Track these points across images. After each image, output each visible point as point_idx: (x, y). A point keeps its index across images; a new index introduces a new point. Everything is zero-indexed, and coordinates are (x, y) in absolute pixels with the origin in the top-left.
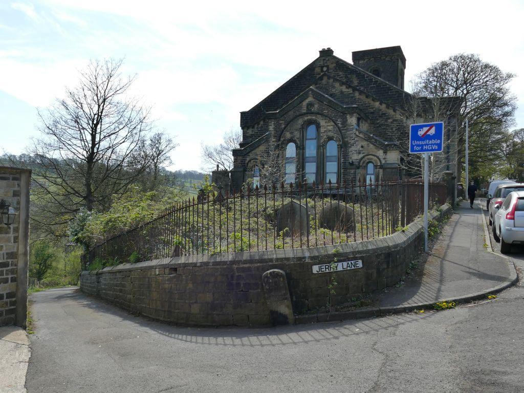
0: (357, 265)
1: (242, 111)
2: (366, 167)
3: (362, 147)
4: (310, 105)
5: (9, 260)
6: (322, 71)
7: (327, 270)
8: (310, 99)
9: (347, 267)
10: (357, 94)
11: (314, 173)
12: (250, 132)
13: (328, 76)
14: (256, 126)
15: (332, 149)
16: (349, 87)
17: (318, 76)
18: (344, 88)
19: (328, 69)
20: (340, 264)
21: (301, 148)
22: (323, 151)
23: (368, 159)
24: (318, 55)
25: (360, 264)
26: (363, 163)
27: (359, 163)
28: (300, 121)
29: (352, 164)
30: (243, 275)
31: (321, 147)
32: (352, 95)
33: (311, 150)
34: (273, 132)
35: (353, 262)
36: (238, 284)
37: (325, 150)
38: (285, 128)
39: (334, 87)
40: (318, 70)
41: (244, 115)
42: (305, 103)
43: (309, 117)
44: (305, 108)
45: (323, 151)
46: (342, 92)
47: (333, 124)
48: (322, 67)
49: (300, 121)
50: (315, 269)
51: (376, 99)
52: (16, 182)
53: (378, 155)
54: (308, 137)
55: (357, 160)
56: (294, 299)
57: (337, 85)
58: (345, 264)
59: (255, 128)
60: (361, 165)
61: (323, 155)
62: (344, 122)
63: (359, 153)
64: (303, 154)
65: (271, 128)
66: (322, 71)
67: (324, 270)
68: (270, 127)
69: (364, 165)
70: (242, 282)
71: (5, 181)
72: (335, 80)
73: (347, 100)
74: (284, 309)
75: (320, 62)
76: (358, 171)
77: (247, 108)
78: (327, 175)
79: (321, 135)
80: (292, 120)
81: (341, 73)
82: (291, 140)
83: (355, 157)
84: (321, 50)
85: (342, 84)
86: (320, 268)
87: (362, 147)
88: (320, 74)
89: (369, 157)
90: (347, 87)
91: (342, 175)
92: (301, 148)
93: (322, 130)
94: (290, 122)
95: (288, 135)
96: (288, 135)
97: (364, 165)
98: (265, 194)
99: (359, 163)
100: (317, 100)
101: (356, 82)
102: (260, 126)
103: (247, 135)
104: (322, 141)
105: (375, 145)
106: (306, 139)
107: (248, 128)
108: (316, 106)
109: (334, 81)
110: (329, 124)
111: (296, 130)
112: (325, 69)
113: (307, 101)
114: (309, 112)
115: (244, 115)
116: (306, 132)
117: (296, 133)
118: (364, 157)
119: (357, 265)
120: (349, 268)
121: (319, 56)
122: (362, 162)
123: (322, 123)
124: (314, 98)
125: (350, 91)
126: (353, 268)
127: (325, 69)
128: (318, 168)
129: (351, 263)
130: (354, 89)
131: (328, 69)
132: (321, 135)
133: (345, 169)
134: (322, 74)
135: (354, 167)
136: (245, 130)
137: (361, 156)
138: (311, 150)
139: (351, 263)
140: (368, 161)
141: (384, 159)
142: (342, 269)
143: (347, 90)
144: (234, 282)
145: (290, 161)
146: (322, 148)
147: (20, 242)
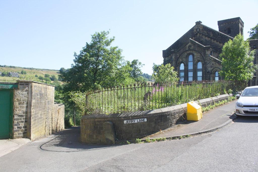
0: (144, 121)
1: (163, 50)
2: (215, 74)
3: (213, 64)
4: (190, 46)
5: (24, 114)
6: (197, 31)
7: (132, 122)
8: (190, 44)
9: (140, 121)
10: (212, 40)
11: (192, 77)
12: (167, 59)
13: (199, 33)
14: (169, 56)
15: (200, 66)
16: (209, 37)
17: (195, 33)
18: (207, 38)
19: (199, 30)
20: (136, 120)
21: (186, 66)
22: (196, 67)
23: (216, 70)
24: (195, 24)
25: (146, 120)
26: (213, 72)
27: (211, 71)
28: (186, 54)
29: (208, 72)
30: (98, 123)
31: (195, 65)
32: (210, 41)
33: (191, 67)
34: (174, 59)
35: (142, 119)
36: (97, 127)
37: (197, 66)
38: (179, 57)
39: (202, 38)
40: (195, 30)
41: (164, 52)
42: (187, 46)
43: (190, 52)
44: (188, 48)
45: (196, 67)
46: (206, 40)
47: (200, 54)
48: (197, 29)
49: (186, 54)
50: (125, 122)
51: (221, 42)
52: (27, 86)
53: (220, 68)
54: (189, 61)
55: (211, 70)
56: (117, 134)
57: (204, 37)
58: (138, 120)
59: (169, 57)
60: (212, 72)
61: (196, 69)
62: (205, 54)
63: (212, 67)
64: (187, 68)
65: (173, 57)
66: (197, 31)
67: (129, 122)
68: (173, 57)
69: (214, 72)
70: (98, 126)
71: (22, 86)
72: (203, 35)
73: (208, 43)
74: (111, 138)
75: (196, 27)
76: (211, 75)
77: (165, 48)
78: (198, 77)
79: (195, 60)
80: (182, 54)
81: (205, 32)
82: (182, 62)
83: (210, 69)
84: (196, 22)
85: (206, 36)
86: (127, 122)
87: (213, 64)
88: (196, 32)
89: (216, 69)
90: (208, 38)
91: (204, 77)
92: (186, 66)
93: (195, 57)
94: (181, 54)
95: (181, 60)
96: (181, 60)
97: (214, 72)
98: (134, 88)
99: (211, 71)
100: (193, 44)
101: (212, 35)
102: (171, 56)
103: (166, 60)
104: (195, 62)
105: (218, 63)
106: (189, 62)
107: (166, 57)
108: (192, 47)
109: (202, 35)
110: (198, 55)
111: (184, 58)
112: (198, 30)
113: (189, 44)
114: (189, 50)
115: (164, 52)
116: (189, 58)
117: (184, 59)
118: (213, 69)
119: (144, 121)
120: (140, 122)
121: (195, 25)
122: (213, 71)
123: (195, 54)
124: (191, 43)
125: (209, 39)
126: (142, 122)
127: (198, 30)
128: (185, 74)
129: (141, 120)
130: (211, 38)
131: (199, 30)
132: (195, 60)
133: (205, 74)
134: (197, 32)
135: (209, 73)
136: (165, 58)
137: (212, 68)
138: (191, 67)
139: (141, 120)
140: (215, 71)
142: (137, 122)
143: (208, 39)
144: (96, 126)
145: (191, 71)
146: (195, 65)
147: (28, 108)
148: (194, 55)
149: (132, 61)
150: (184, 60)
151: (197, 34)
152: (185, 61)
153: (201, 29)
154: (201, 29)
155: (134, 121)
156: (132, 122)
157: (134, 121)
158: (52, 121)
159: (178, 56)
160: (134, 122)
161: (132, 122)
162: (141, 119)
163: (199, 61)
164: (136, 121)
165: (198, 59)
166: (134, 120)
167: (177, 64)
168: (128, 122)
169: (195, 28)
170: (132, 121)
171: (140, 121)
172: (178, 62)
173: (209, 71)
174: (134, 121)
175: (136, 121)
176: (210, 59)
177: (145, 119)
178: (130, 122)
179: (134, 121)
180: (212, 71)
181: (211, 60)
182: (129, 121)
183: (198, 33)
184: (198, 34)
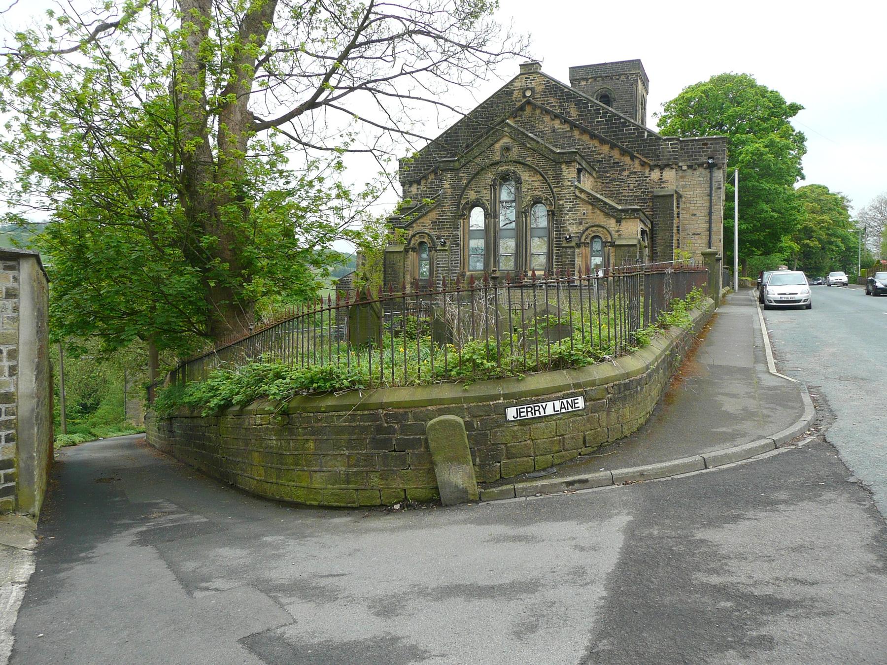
0: (577, 405)
7: (537, 413)
9: (561, 408)
14: (423, 182)
15: (540, 217)
18: (557, 124)
20: (550, 404)
25: (580, 403)
28: (489, 176)
31: (523, 214)
32: (568, 134)
35: (569, 400)
38: (467, 184)
47: (541, 178)
50: (511, 413)
55: (577, 233)
58: (558, 404)
60: (583, 240)
63: (581, 223)
66: (525, 96)
67: (525, 414)
81: (552, 100)
86: (519, 412)
92: (491, 215)
93: (524, 188)
96: (472, 195)
112: (528, 94)
117: (485, 191)
118: (587, 229)
119: (577, 405)
120: (563, 410)
123: (525, 176)
125: (567, 127)
126: (570, 409)
132: (523, 195)
133: (559, 247)
136: (406, 187)
137: (582, 228)
138: (507, 217)
140: (593, 235)
141: (618, 231)
148: (519, 179)
149: (693, 83)
150: (486, 195)
151: (522, 108)
152: (487, 200)
153: (539, 89)
154: (539, 89)
155: (544, 409)
156: (537, 413)
157: (542, 410)
158: (564, 540)
159: (465, 182)
160: (543, 414)
161: (535, 411)
162: (564, 401)
163: (537, 201)
164: (550, 408)
165: (536, 193)
166: (544, 404)
167: (458, 207)
168: (520, 412)
169: (517, 84)
170: (537, 408)
171: (565, 408)
172: (463, 202)
173: (572, 235)
174: (542, 410)
175: (550, 408)
176: (578, 193)
177: (580, 398)
178: (530, 414)
179: (544, 409)
180: (582, 236)
181: (580, 198)
182: (525, 410)
183: (528, 103)
184: (528, 109)
